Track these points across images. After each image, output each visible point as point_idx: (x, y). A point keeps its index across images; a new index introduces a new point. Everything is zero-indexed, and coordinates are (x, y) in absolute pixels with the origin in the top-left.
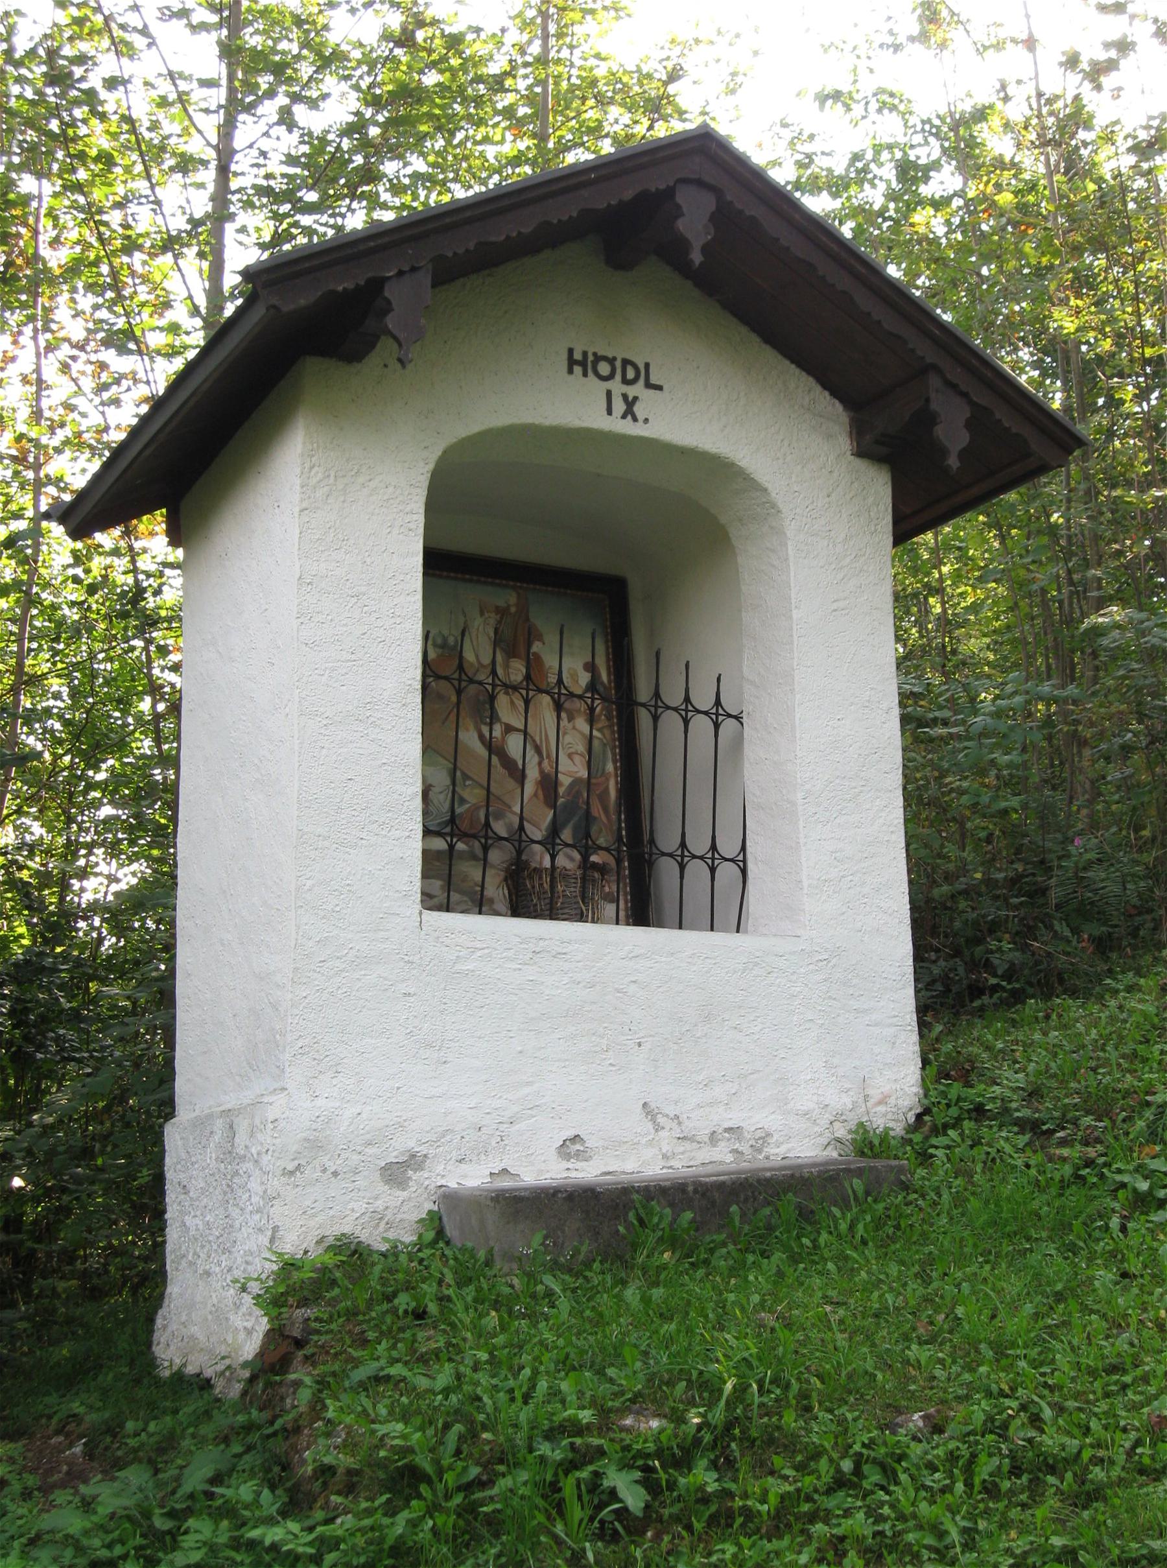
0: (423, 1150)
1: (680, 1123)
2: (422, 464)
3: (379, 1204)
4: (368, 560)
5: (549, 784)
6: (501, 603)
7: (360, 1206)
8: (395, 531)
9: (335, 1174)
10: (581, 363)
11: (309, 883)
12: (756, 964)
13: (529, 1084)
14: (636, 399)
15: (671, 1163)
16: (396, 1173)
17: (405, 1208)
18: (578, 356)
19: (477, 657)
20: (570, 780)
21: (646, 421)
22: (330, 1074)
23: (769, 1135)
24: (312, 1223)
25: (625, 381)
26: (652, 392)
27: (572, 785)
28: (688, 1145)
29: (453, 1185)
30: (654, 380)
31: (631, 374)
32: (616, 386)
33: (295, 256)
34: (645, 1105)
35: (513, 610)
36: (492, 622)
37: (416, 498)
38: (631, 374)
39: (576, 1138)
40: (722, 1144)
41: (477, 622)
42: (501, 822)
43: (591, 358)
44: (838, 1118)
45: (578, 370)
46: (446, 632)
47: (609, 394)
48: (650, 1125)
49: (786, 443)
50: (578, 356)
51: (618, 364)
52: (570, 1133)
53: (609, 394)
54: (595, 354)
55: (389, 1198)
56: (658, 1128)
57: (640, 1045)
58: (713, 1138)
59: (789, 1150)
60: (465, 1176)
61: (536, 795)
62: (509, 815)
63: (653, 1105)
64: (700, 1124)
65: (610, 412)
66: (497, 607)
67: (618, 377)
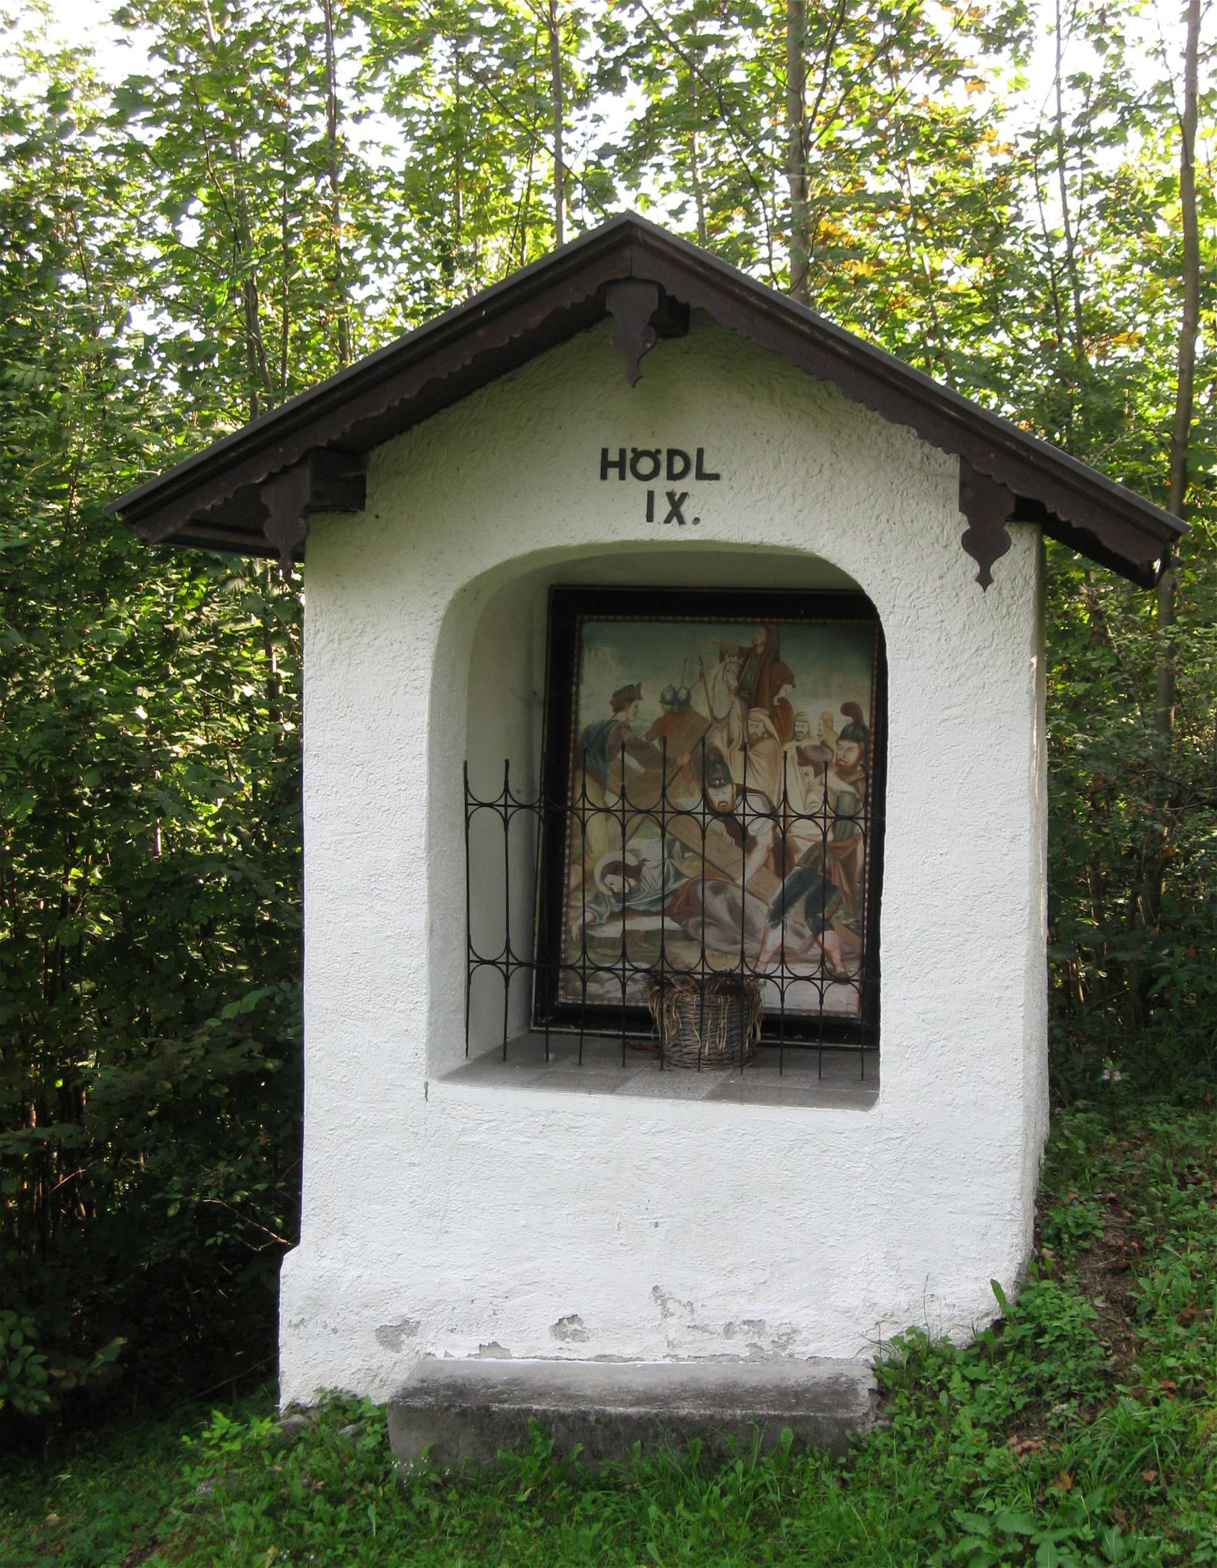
0: (415, 1317)
1: (692, 1311)
2: (429, 613)
3: (374, 1363)
4: (373, 726)
5: (782, 851)
6: (746, 644)
7: (356, 1362)
8: (401, 691)
9: (335, 1331)
10: (615, 465)
11: (319, 1054)
12: (807, 1142)
13: (529, 1259)
14: (684, 495)
15: (677, 1352)
16: (390, 1336)
17: (397, 1369)
18: (613, 456)
19: (711, 710)
20: (810, 844)
21: (697, 520)
22: (338, 1236)
23: (795, 1331)
24: (314, 1373)
25: (672, 476)
26: (705, 483)
27: (811, 850)
28: (698, 1335)
29: (440, 1355)
30: (708, 468)
31: (679, 466)
32: (661, 485)
33: (560, 256)
34: (656, 1288)
35: (760, 650)
36: (734, 668)
37: (422, 652)
38: (679, 466)
39: (573, 1318)
40: (739, 1336)
41: (716, 669)
42: (721, 897)
43: (629, 455)
44: (889, 1317)
45: (613, 473)
46: (677, 685)
47: (651, 495)
48: (658, 1310)
49: (884, 518)
50: (613, 456)
51: (663, 458)
52: (569, 1312)
53: (651, 495)
54: (634, 450)
55: (384, 1358)
56: (666, 1314)
57: (657, 1225)
58: (729, 1330)
59: (820, 1350)
60: (454, 1346)
61: (766, 864)
62: (731, 888)
63: (664, 1290)
64: (715, 1314)
65: (650, 518)
66: (741, 649)
67: (663, 472)
